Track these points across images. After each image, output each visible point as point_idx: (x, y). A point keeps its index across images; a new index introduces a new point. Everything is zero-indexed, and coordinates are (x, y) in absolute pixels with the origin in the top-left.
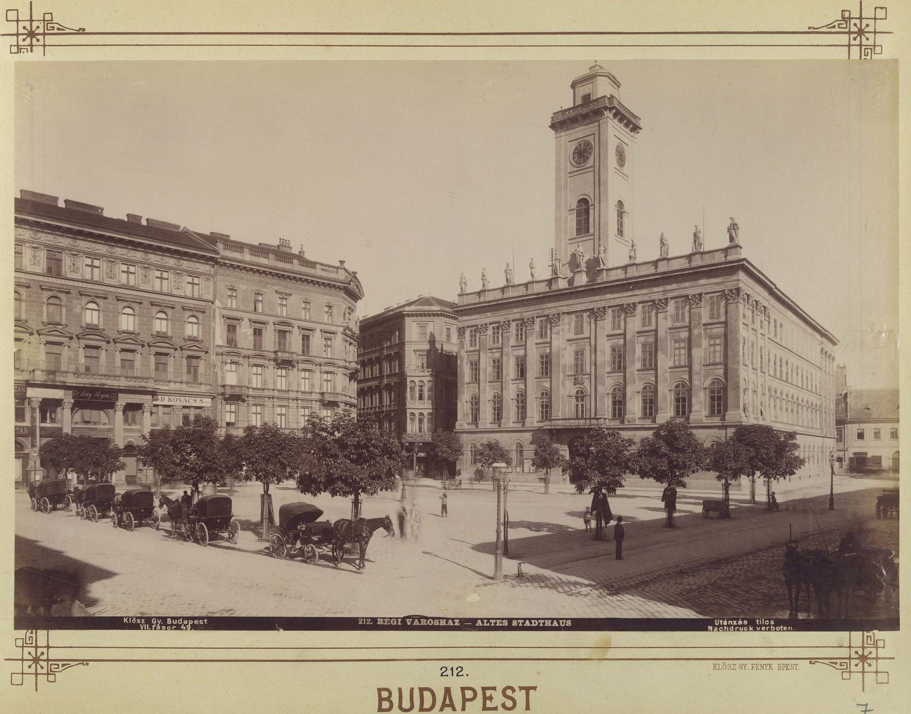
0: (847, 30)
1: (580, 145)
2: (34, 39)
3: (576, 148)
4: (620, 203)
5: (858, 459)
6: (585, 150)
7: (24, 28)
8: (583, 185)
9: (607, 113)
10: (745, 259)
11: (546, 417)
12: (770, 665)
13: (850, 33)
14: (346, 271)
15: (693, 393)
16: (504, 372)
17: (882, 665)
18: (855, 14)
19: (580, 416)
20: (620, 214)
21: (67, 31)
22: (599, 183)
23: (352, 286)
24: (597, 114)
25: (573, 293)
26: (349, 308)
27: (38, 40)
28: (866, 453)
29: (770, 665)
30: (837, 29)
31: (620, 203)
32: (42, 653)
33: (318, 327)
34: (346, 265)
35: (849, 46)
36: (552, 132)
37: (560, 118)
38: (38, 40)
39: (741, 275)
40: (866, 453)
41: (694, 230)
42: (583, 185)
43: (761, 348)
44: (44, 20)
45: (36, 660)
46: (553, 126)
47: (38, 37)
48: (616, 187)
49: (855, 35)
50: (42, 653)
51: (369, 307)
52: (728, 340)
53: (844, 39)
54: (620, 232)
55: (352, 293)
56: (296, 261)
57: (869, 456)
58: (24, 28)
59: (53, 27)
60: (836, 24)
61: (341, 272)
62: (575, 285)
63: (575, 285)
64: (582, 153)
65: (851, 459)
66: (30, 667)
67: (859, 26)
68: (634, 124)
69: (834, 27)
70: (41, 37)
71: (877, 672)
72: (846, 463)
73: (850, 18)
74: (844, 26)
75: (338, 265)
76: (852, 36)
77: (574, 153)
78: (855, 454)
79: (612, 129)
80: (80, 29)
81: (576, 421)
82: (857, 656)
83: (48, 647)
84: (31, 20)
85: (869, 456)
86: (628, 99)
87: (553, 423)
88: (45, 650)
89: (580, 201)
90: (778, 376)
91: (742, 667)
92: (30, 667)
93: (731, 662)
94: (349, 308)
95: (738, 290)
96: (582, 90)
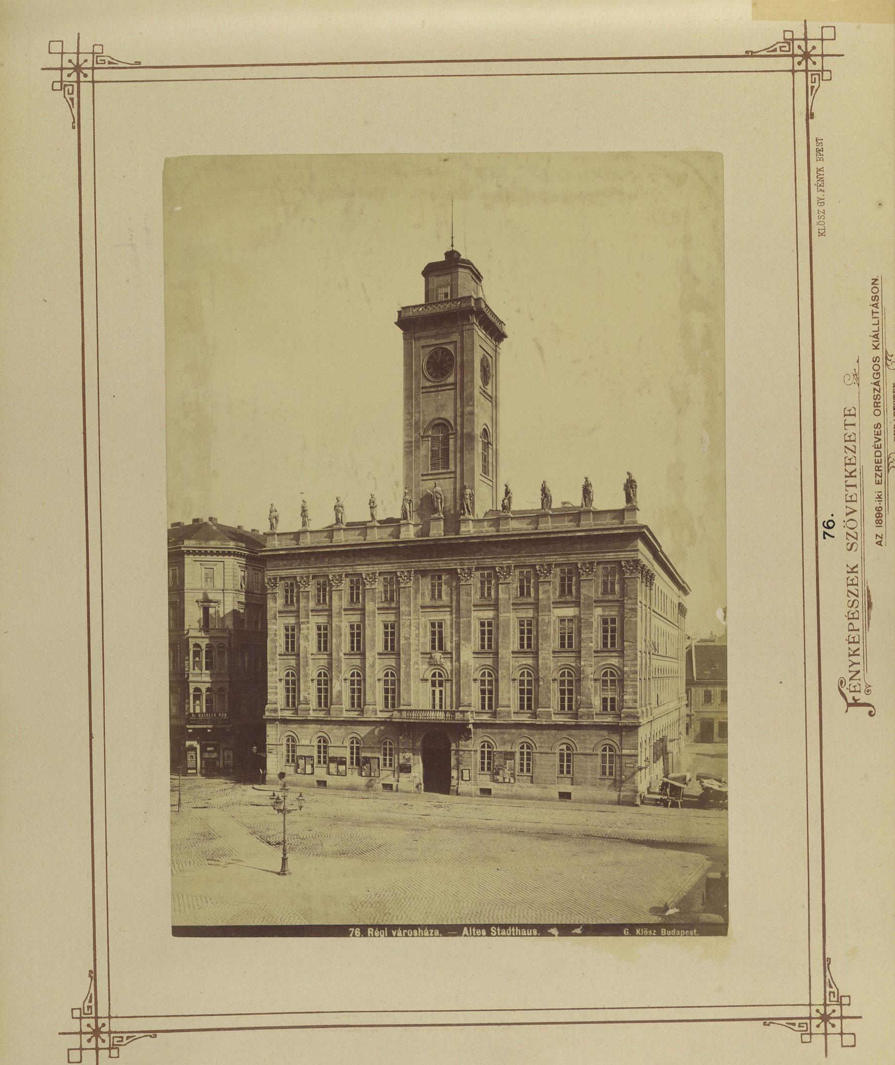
0: (75, 85)
2: (103, 1029)
7: (89, 1041)
11: (393, 705)
12: (819, 170)
13: (78, 82)
17: (814, 32)
18: (56, 75)
20: (486, 445)
21: (92, 991)
27: (104, 1025)
29: (819, 170)
30: (75, 96)
32: (799, 63)
35: (93, 82)
38: (104, 1025)
41: (583, 482)
44: (93, 53)
45: (806, 56)
47: (100, 1025)
49: (81, 75)
50: (799, 63)
53: (86, 88)
58: (89, 1041)
59: (89, 1007)
60: (68, 97)
66: (814, 48)
67: (70, 71)
69: (72, 99)
70: (100, 1022)
71: (842, 1034)
73: (61, 82)
74: (71, 88)
76: (82, 78)
80: (90, 976)
82: (818, 1015)
83: (793, 71)
84: (81, 1033)
88: (797, 67)
91: (821, 202)
92: (814, 48)
93: (814, 216)
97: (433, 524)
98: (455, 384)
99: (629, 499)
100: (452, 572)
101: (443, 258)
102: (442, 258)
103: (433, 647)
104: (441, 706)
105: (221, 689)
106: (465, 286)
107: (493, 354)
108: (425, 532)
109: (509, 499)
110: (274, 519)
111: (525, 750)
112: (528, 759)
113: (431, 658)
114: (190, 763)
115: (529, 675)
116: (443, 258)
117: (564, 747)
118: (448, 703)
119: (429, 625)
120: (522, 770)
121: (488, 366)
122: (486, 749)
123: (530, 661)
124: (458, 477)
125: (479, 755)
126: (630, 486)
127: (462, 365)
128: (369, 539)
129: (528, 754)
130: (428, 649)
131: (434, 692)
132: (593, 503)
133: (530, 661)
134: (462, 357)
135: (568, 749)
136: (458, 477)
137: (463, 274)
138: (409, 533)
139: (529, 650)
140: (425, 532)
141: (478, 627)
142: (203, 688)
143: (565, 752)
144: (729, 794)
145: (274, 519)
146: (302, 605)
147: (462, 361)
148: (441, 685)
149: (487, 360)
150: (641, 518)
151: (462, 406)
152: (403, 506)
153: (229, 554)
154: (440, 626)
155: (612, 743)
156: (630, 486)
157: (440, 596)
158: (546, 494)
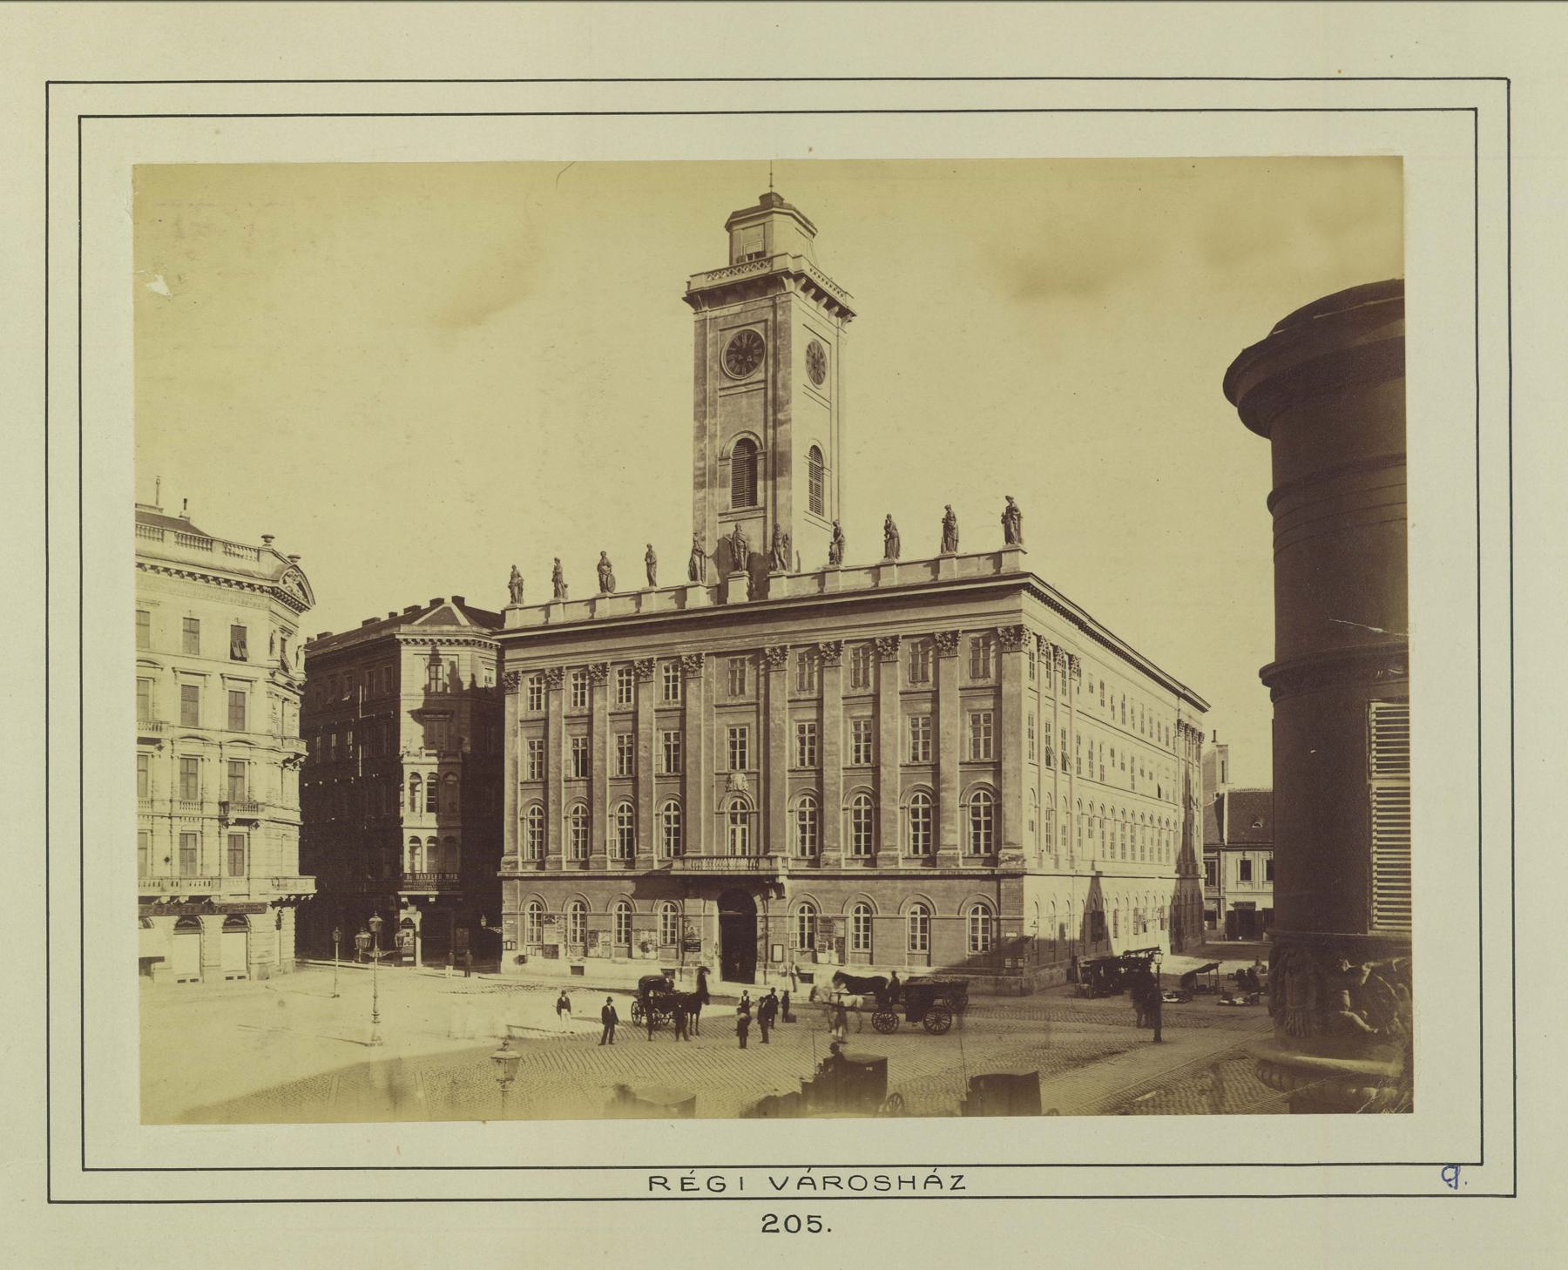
1: (740, 338)
3: (733, 344)
4: (816, 451)
5: (1241, 912)
6: (748, 351)
8: (742, 413)
9: (790, 285)
10: (1027, 575)
11: (677, 852)
14: (276, 555)
15: (944, 815)
16: (596, 763)
19: (739, 853)
20: (817, 472)
22: (776, 405)
23: (291, 586)
24: (771, 283)
25: (721, 617)
26: (283, 629)
28: (1253, 904)
31: (816, 451)
33: (168, 663)
34: (275, 545)
36: (689, 309)
37: (703, 283)
39: (1026, 600)
40: (1253, 904)
41: (944, 513)
42: (742, 413)
43: (1064, 733)
46: (695, 299)
48: (805, 423)
51: (338, 612)
52: (993, 727)
54: (816, 506)
55: (291, 594)
56: (170, 536)
57: (1258, 908)
61: (267, 558)
62: (730, 601)
63: (730, 601)
64: (747, 354)
65: (1229, 914)
68: (841, 308)
72: (1221, 922)
75: (260, 543)
77: (729, 353)
78: (1236, 904)
79: (802, 313)
81: (732, 862)
85: (1258, 908)
86: (828, 260)
87: (688, 864)
89: (740, 443)
90: (1097, 778)
94: (283, 629)
95: (1019, 629)
96: (751, 239)
97: (732, 584)
98: (765, 381)
99: (1009, 538)
100: (758, 653)
101: (757, 203)
102: (1253, 457)
103: (734, 767)
104: (744, 851)
105: (449, 840)
106: (784, 237)
107: (833, 340)
108: (720, 592)
109: (840, 543)
110: (516, 586)
111: (862, 915)
112: (866, 929)
113: (729, 781)
114: (406, 948)
115: (925, 800)
116: (757, 203)
117: (917, 908)
118: (754, 848)
119: (727, 734)
120: (857, 945)
121: (822, 356)
122: (806, 915)
123: (988, 779)
124: (770, 515)
125: (796, 922)
126: (1011, 516)
127: (775, 355)
128: (644, 610)
129: (866, 920)
130: (727, 768)
131: (734, 832)
132: (959, 545)
133: (988, 779)
134: (775, 341)
135: (923, 912)
136: (770, 515)
137: (781, 225)
138: (700, 598)
139: (987, 760)
140: (720, 592)
141: (795, 732)
142: (424, 836)
143: (919, 917)
144: (690, 1121)
145: (516, 586)
146: (552, 709)
147: (775, 347)
148: (743, 821)
149: (820, 347)
150: (1024, 563)
151: (775, 413)
152: (692, 559)
153: (467, 643)
154: (743, 733)
155: (986, 902)
156: (1011, 516)
157: (742, 690)
158: (892, 537)
